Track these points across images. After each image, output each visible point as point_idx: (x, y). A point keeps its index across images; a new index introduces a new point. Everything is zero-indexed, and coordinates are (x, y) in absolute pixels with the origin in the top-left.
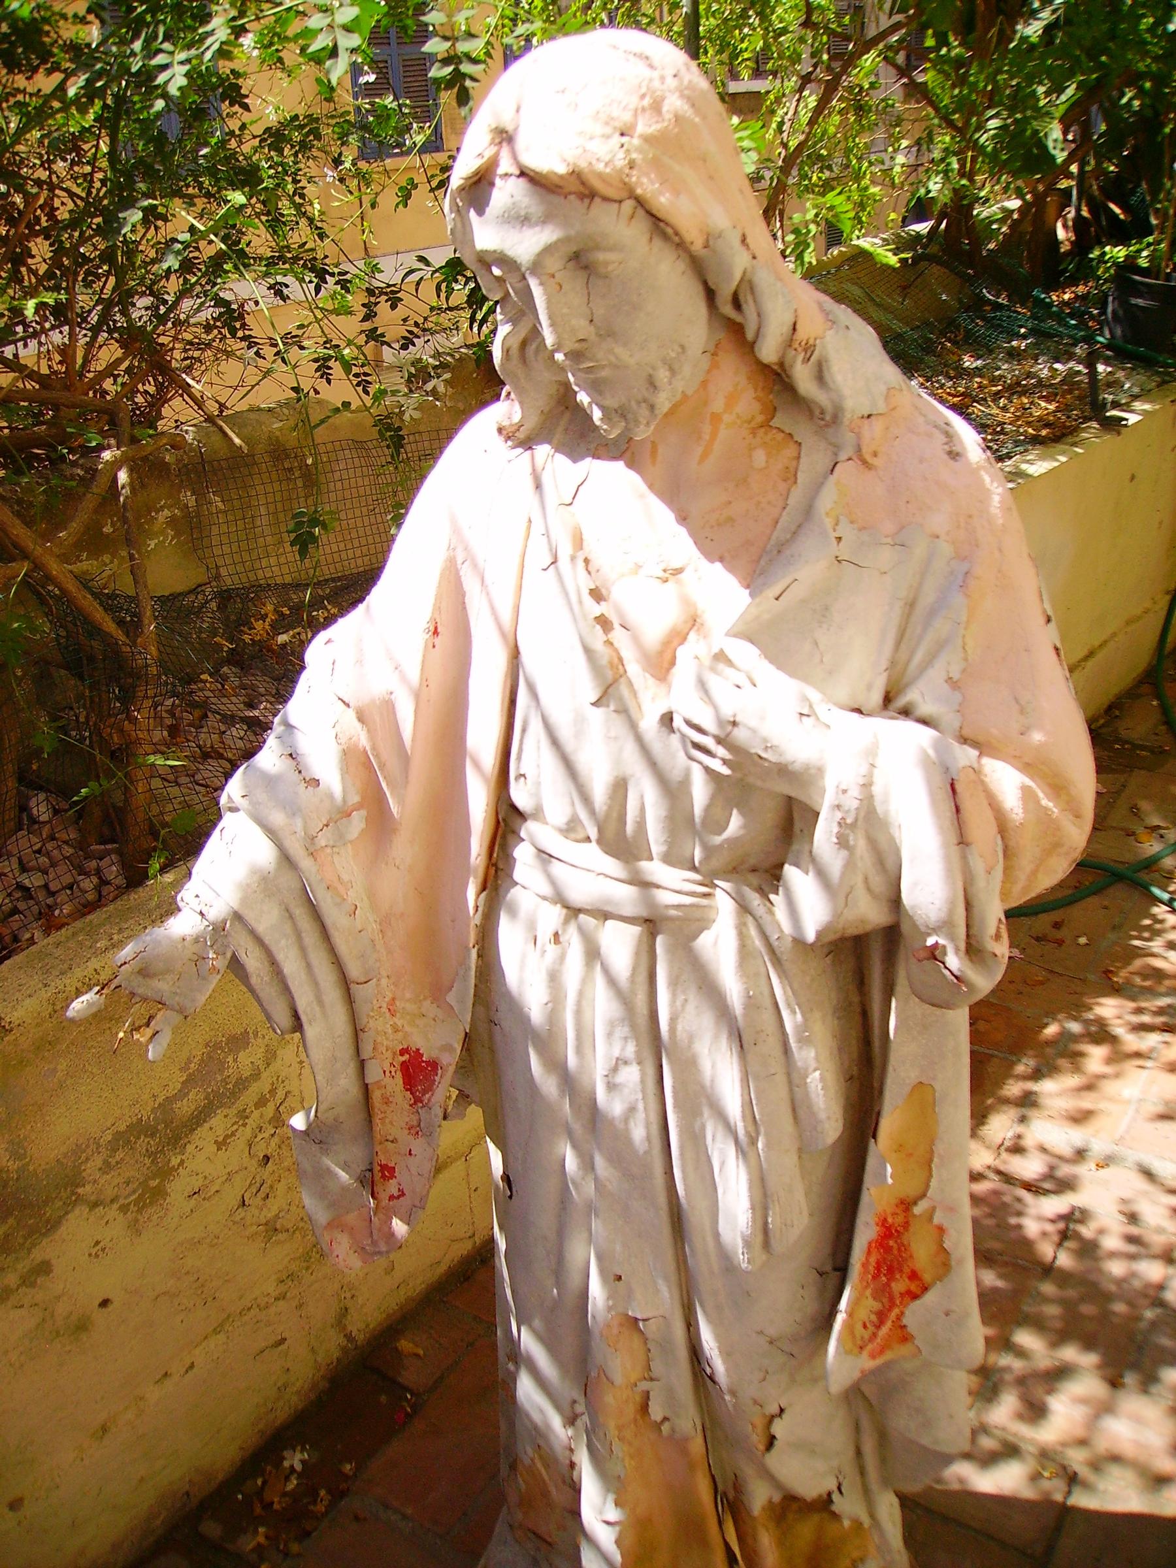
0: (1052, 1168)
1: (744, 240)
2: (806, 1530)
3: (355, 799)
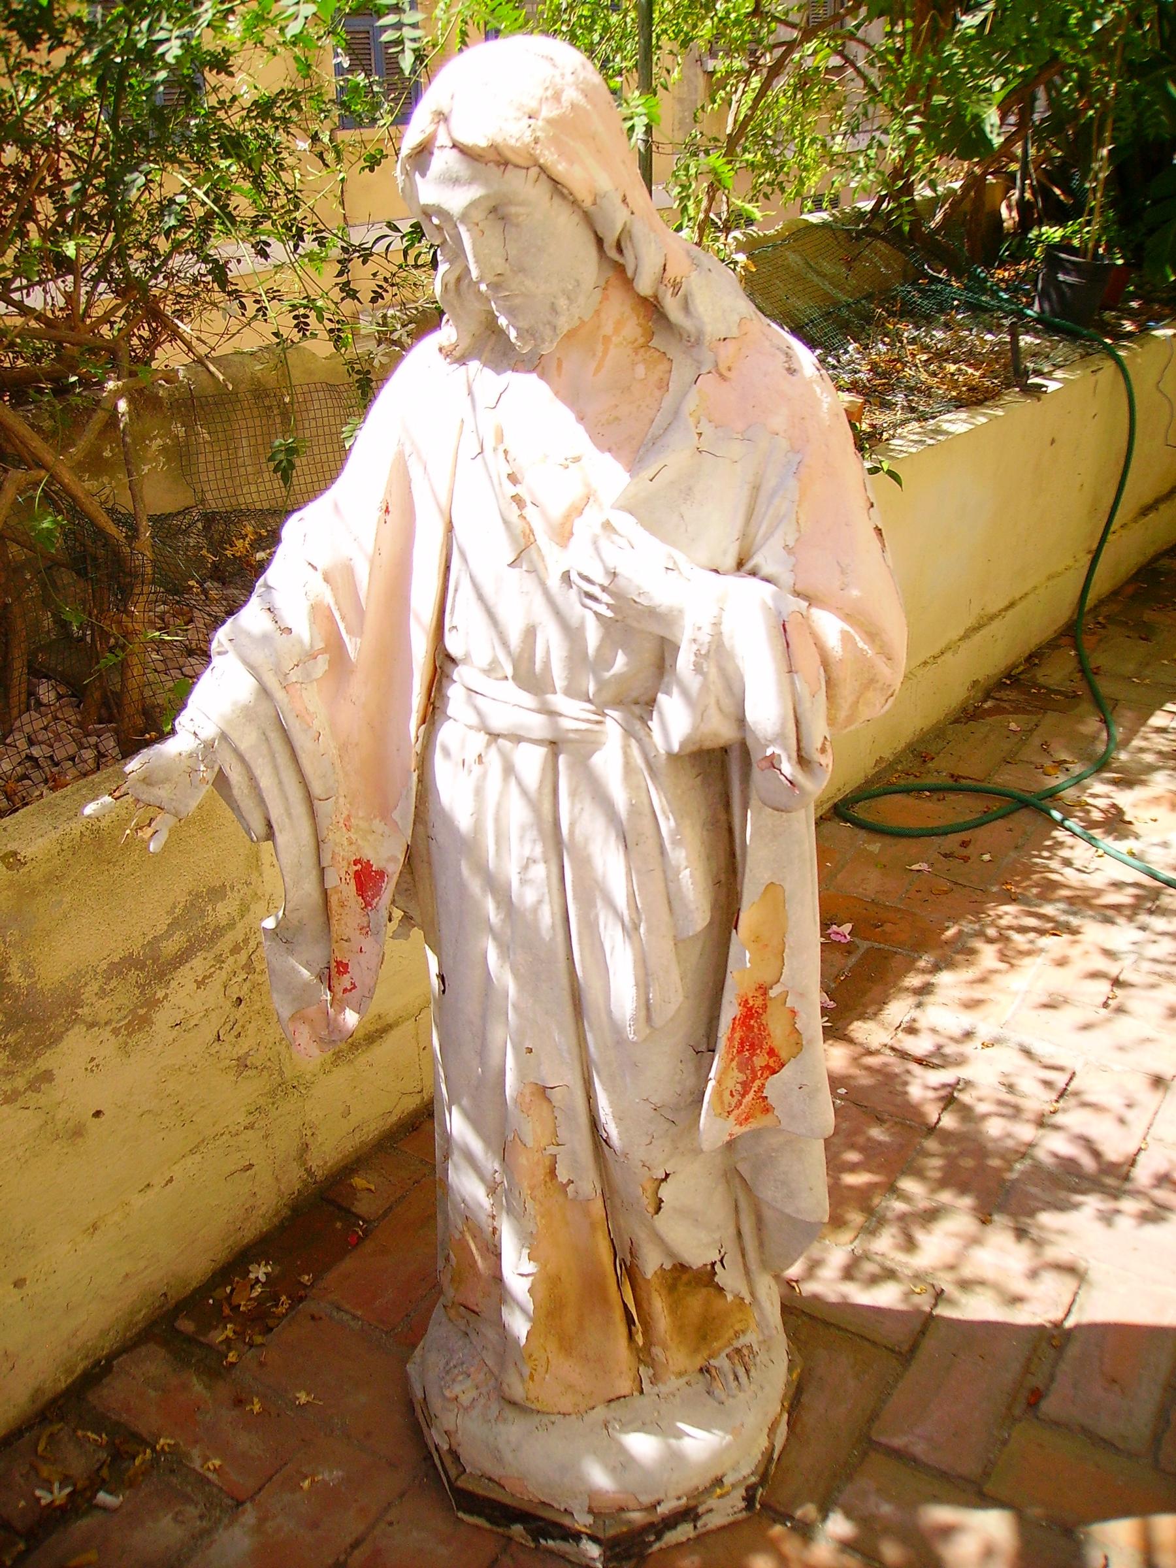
0: (939, 1047)
1: (624, 200)
2: (695, 1302)
3: (320, 645)
